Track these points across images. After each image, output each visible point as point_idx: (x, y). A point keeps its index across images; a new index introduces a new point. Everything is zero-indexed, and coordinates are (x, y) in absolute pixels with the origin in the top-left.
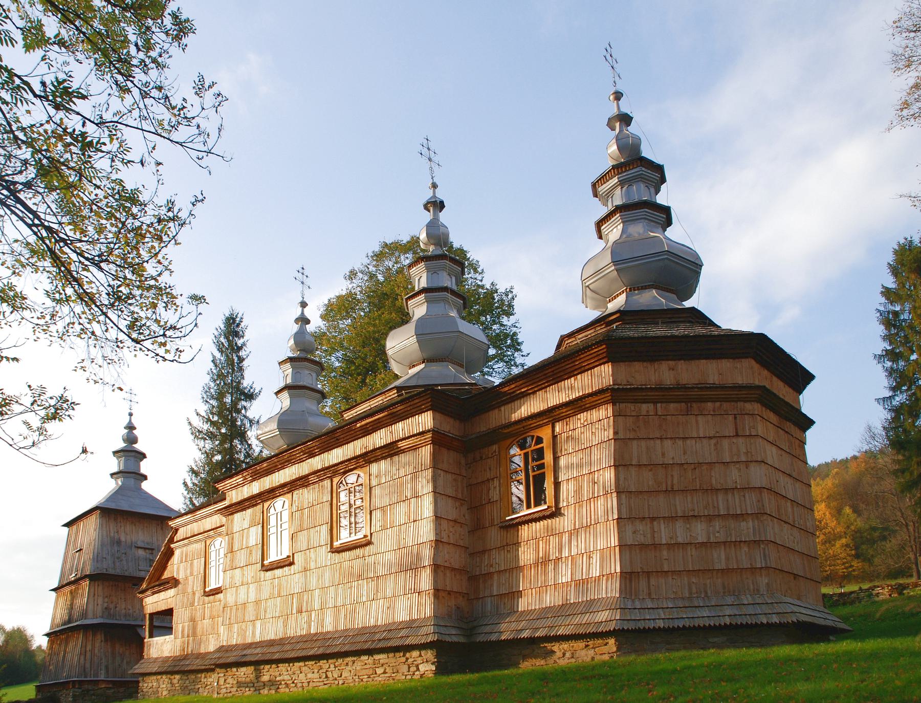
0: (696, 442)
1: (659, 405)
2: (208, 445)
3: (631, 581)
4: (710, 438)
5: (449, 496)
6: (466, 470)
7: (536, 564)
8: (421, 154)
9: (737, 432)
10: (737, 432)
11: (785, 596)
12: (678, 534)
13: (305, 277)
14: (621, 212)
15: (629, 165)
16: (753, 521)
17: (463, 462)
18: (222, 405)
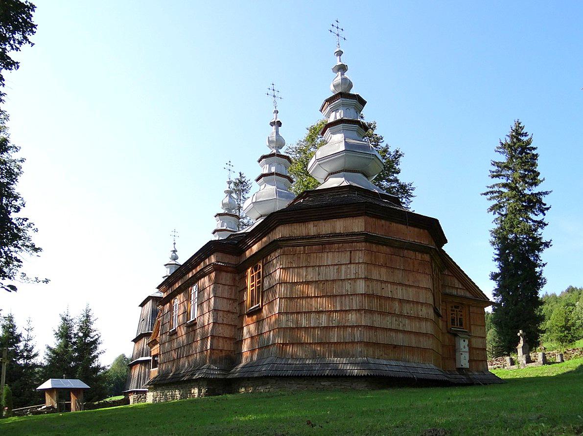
5: (225, 298)
7: (258, 335)
14: (329, 127)
16: (356, 314)
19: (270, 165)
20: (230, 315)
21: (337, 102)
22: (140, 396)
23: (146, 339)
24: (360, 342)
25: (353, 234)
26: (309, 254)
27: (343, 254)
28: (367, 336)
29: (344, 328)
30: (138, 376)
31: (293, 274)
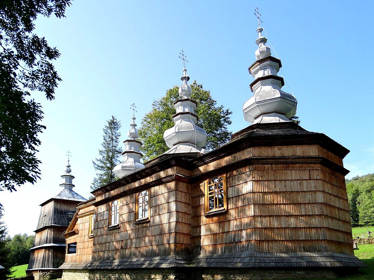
0: (291, 182)
1: (273, 165)
2: (102, 172)
3: (260, 244)
4: (298, 180)
5: (183, 202)
6: (191, 191)
8: (180, 57)
9: (310, 178)
10: (310, 178)
11: (334, 253)
12: (282, 223)
13: (135, 107)
15: (264, 60)
17: (190, 187)
18: (108, 156)
19: (184, 107)
20: (187, 216)
21: (266, 63)
22: (45, 274)
23: (49, 231)
24: (325, 240)
25: (312, 158)
26: (276, 171)
27: (304, 172)
28: (329, 235)
29: (309, 229)
30: (43, 258)
31: (263, 185)
